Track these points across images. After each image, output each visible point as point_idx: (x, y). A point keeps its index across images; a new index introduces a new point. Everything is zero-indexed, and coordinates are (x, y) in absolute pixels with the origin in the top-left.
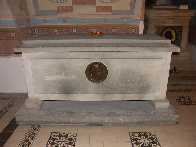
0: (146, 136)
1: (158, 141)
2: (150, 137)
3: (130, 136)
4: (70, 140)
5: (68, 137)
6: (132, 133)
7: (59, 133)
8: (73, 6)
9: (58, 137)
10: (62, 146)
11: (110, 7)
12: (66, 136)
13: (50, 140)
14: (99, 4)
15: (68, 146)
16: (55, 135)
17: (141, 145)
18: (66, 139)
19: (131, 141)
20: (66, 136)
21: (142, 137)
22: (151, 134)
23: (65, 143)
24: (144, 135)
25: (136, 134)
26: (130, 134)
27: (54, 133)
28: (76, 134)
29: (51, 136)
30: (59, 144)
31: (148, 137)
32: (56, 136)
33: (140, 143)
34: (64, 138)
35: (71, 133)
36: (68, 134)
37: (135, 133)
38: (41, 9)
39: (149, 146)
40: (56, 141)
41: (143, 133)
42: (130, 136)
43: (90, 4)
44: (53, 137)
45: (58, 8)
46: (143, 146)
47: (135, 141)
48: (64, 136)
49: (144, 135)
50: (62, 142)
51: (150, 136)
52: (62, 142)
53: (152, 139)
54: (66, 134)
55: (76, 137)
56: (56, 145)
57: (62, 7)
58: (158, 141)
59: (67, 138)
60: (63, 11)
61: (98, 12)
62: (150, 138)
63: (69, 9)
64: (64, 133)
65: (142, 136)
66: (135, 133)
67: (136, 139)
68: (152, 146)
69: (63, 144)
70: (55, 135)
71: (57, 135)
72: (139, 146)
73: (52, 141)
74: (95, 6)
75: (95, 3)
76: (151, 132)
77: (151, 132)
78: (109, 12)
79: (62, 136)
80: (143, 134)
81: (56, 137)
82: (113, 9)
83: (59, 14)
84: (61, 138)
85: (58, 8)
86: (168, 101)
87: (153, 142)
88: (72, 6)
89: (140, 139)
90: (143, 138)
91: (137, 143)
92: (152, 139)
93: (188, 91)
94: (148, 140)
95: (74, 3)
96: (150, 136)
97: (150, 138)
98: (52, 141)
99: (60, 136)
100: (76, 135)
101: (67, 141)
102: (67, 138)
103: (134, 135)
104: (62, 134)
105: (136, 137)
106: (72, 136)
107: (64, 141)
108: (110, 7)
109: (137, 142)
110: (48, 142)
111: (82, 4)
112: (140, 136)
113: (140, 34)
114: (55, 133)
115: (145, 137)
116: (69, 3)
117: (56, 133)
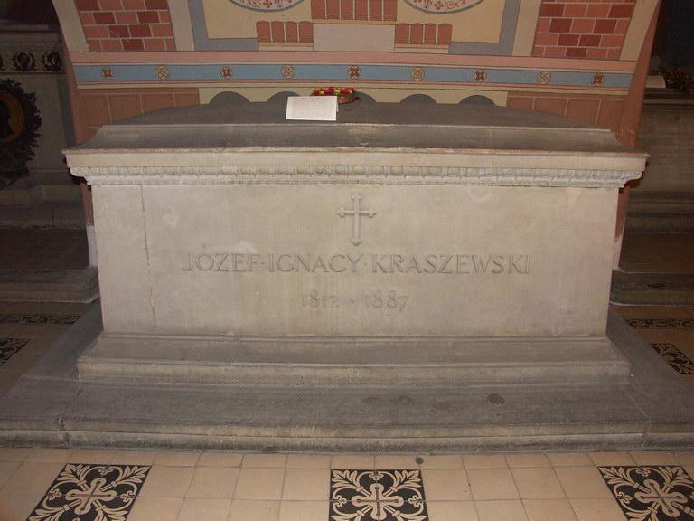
0: (387, 482)
1: (615, 496)
3: (332, 483)
4: (121, 489)
5: (395, 484)
7: (359, 472)
8: (315, 21)
10: (385, 520)
11: (446, 29)
12: (112, 476)
14: (406, 14)
15: (405, 516)
17: (653, 511)
18: (109, 487)
19: (328, 498)
20: (112, 476)
21: (372, 487)
22: (408, 476)
23: (100, 501)
26: (335, 473)
27: (340, 473)
28: (147, 469)
30: (77, 506)
32: (352, 483)
33: (360, 508)
34: (104, 481)
35: (400, 471)
36: (120, 469)
38: (214, 30)
39: (683, 516)
40: (109, 496)
41: (644, 469)
42: (607, 480)
43: (376, 17)
44: (68, 478)
45: (261, 26)
46: (660, 513)
48: (104, 477)
49: (650, 477)
51: (672, 480)
52: (377, 501)
53: (406, 494)
54: (382, 476)
55: (143, 479)
56: (363, 515)
57: (277, 24)
58: (615, 496)
59: (67, 508)
60: (279, 39)
61: (399, 43)
62: (400, 493)
63: (304, 33)
64: (376, 472)
65: (374, 482)
66: (351, 471)
67: (629, 490)
68: (398, 517)
69: (92, 505)
70: (74, 473)
71: (83, 473)
72: (649, 516)
74: (392, 22)
75: (391, 14)
76: (62, 468)
77: (409, 471)
78: (439, 46)
79: (99, 475)
81: (76, 481)
82: (456, 36)
83: (263, 47)
84: (93, 483)
85: (261, 26)
87: (349, 498)
88: (310, 20)
90: (374, 491)
91: (348, 508)
92: (406, 494)
93: (644, 324)
94: (669, 492)
95: (317, 13)
96: (672, 480)
97: (400, 493)
99: (366, 482)
100: (146, 473)
101: (73, 498)
102: (67, 508)
103: (616, 476)
104: (100, 471)
106: (132, 475)
107: (100, 493)
108: (446, 29)
109: (405, 498)
111: (361, 16)
112: (638, 478)
113: (205, 106)
114: (76, 465)
115: (382, 488)
116: (302, 13)
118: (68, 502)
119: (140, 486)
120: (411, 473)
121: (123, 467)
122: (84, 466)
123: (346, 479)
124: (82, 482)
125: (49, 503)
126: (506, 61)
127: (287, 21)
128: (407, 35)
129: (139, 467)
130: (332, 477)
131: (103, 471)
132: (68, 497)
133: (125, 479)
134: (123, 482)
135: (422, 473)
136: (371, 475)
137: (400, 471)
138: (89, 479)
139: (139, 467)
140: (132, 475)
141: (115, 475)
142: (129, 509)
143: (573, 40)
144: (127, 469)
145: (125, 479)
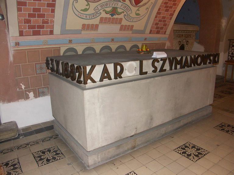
2: (43, 160)
5: (10, 164)
6: (62, 158)
9: (192, 156)
11: (132, 26)
12: (198, 149)
13: (201, 157)
16: (194, 158)
18: (186, 151)
24: (50, 160)
25: (58, 159)
27: (193, 160)
29: (198, 160)
31: (52, 151)
32: (193, 157)
36: (201, 149)
37: (60, 159)
42: (63, 155)
44: (187, 145)
45: (84, 25)
47: (58, 152)
48: (196, 149)
49: (50, 160)
50: (191, 151)
55: (206, 154)
59: (185, 151)
64: (52, 161)
66: (60, 159)
67: (57, 154)
69: (191, 153)
70: (194, 158)
71: (191, 145)
73: (199, 156)
80: (51, 161)
85: (84, 25)
86: (164, 54)
89: (53, 156)
90: (50, 157)
98: (199, 156)
102: (185, 151)
105: (58, 156)
106: (179, 150)
108: (132, 26)
110: (203, 156)
114: (192, 160)
117: (191, 159)
118: (186, 150)
119: (204, 155)
120: (42, 165)
121: (202, 149)
122: (192, 144)
123: (16, 172)
124: (190, 147)
125: (181, 148)
126: (143, 43)
127: (91, 24)
128: (123, 28)
129: (206, 151)
130: (33, 155)
131: (196, 147)
132: (186, 149)
133: (201, 152)
134: (182, 150)
135: (38, 166)
136: (53, 160)
137: (45, 164)
138: (192, 147)
139: (14, 159)
140: (179, 150)
141: (199, 149)
142: (199, 159)
143: (33, 27)
144: (203, 150)
145: (201, 152)
